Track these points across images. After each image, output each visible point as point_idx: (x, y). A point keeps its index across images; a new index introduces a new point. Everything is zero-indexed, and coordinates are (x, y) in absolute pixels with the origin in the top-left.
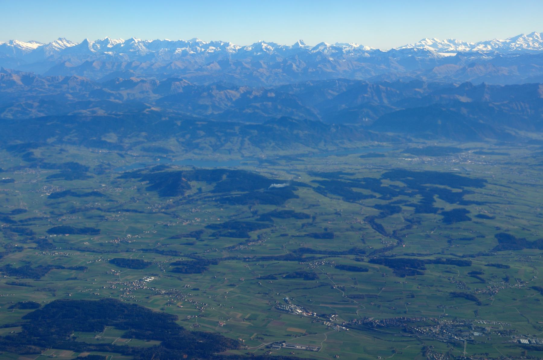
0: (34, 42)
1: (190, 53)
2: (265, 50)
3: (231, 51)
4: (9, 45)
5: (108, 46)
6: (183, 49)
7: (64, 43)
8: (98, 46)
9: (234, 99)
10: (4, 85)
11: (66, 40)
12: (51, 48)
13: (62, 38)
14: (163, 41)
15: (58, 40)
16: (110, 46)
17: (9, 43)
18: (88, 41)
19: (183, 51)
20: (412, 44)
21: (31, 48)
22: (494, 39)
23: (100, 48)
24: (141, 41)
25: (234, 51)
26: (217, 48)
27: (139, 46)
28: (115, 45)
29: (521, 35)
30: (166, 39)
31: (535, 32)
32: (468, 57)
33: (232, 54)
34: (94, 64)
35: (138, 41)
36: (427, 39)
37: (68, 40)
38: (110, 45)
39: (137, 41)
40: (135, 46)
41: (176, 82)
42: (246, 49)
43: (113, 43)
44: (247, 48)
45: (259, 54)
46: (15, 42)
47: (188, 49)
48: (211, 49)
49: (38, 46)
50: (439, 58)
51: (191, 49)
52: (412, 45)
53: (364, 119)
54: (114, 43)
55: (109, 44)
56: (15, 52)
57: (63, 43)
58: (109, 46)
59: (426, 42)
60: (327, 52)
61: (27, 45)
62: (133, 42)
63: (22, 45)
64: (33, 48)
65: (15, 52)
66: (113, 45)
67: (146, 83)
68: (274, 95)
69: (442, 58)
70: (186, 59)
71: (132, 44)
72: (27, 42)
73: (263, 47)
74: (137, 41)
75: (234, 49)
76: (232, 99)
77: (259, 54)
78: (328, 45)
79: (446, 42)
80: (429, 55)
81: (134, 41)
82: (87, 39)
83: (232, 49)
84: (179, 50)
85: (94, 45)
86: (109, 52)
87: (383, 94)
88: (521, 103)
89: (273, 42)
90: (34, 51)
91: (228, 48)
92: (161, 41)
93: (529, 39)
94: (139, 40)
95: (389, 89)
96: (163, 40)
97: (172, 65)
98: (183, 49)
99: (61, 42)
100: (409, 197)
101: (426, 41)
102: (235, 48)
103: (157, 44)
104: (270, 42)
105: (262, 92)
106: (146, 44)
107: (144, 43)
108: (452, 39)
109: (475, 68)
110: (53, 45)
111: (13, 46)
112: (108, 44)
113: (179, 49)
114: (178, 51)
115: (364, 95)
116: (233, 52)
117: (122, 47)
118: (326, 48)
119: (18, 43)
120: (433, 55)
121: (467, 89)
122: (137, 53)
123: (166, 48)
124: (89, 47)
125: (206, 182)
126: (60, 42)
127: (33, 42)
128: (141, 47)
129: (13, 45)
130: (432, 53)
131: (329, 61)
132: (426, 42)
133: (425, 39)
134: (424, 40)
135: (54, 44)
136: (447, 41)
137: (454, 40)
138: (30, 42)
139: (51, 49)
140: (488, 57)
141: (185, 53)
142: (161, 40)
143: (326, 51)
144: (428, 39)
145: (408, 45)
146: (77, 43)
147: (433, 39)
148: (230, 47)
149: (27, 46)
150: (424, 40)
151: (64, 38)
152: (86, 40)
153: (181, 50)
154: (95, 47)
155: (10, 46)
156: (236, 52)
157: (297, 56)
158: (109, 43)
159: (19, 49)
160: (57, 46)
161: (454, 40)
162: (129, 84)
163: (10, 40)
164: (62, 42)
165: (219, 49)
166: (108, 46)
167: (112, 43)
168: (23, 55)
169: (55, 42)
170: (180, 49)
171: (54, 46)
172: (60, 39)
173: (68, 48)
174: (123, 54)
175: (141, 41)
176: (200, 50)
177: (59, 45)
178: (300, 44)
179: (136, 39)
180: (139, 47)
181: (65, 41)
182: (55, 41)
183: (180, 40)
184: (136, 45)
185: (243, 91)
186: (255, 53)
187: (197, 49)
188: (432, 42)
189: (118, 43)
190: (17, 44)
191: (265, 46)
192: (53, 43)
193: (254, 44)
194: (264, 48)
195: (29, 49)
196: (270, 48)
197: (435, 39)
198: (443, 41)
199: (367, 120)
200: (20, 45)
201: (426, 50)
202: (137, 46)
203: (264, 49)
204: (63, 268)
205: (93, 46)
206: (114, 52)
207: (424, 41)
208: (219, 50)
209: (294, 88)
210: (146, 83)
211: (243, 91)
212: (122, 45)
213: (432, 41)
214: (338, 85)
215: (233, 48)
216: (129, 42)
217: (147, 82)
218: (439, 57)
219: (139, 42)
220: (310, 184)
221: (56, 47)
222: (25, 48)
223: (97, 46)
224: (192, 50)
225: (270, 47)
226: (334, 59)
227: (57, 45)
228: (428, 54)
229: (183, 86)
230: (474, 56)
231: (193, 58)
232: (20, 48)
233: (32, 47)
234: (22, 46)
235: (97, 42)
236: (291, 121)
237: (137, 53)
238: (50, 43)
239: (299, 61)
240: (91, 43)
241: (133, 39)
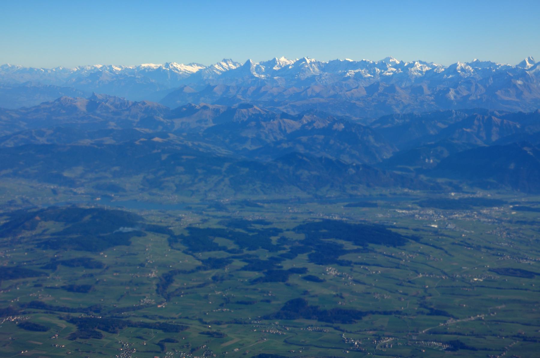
0: (196, 65)
1: (366, 76)
2: (459, 72)
3: (416, 74)
4: (164, 68)
5: (274, 68)
6: (357, 71)
7: (229, 65)
8: (262, 68)
9: (289, 131)
10: (64, 112)
11: (232, 62)
12: (211, 71)
13: (228, 60)
14: (343, 61)
15: (223, 61)
16: (277, 68)
17: (165, 67)
18: (251, 62)
19: (356, 73)
21: (189, 72)
23: (264, 70)
24: (315, 61)
25: (420, 74)
26: (397, 70)
27: (310, 68)
28: (283, 67)
30: (346, 59)
33: (416, 77)
34: (215, 89)
35: (311, 61)
37: (234, 61)
38: (277, 66)
39: (310, 62)
40: (305, 68)
41: (242, 110)
42: (436, 70)
43: (281, 65)
44: (438, 69)
45: (451, 76)
46: (172, 65)
47: (364, 71)
48: (389, 71)
49: (199, 69)
51: (367, 71)
53: (427, 160)
54: (282, 64)
55: (276, 66)
56: (169, 77)
57: (229, 65)
58: (276, 68)
61: (186, 69)
62: (304, 62)
63: (180, 69)
64: (192, 72)
65: (169, 77)
66: (281, 66)
67: (208, 110)
68: (343, 127)
70: (345, 84)
71: (302, 64)
72: (187, 65)
73: (458, 68)
74: (310, 62)
75: (420, 71)
76: (285, 131)
77: (451, 76)
81: (306, 61)
82: (250, 60)
83: (418, 71)
84: (351, 73)
85: (258, 66)
86: (261, 75)
87: (494, 128)
89: (490, 61)
90: (193, 75)
91: (413, 69)
92: (340, 61)
94: (313, 60)
95: (505, 121)
96: (343, 60)
97: (308, 90)
98: (357, 71)
99: (225, 64)
100: (268, 251)
102: (422, 70)
103: (334, 65)
104: (487, 61)
105: (329, 122)
106: (322, 66)
107: (319, 64)
110: (215, 68)
111: (168, 69)
112: (275, 65)
113: (351, 72)
114: (350, 73)
115: (465, 129)
116: (418, 75)
117: (290, 69)
119: (175, 66)
122: (296, 76)
123: (345, 70)
124: (251, 69)
126: (224, 64)
127: (194, 65)
128: (314, 69)
129: (169, 68)
131: (515, 86)
135: (216, 66)
138: (191, 65)
139: (210, 72)
141: (358, 76)
142: (341, 60)
146: (120, 67)
148: (416, 68)
149: (186, 70)
151: (231, 60)
152: (248, 62)
153: (354, 72)
154: (258, 69)
155: (165, 69)
156: (422, 74)
157: (492, 79)
158: (277, 64)
159: (176, 73)
160: (219, 69)
162: (191, 110)
163: (167, 63)
164: (227, 64)
165: (400, 71)
166: (274, 68)
167: (280, 64)
168: (179, 80)
169: (218, 65)
170: (353, 71)
171: (216, 69)
172: (225, 61)
173: (231, 70)
174: (279, 77)
175: (315, 61)
176: (380, 72)
177: (223, 68)
178: (527, 62)
179: (308, 59)
180: (311, 69)
181: (231, 62)
182: (218, 63)
183: (364, 60)
184: (307, 66)
185: (307, 121)
186: (445, 76)
187: (375, 70)
189: (159, 66)
190: (174, 67)
191: (461, 67)
192: (215, 65)
194: (460, 69)
195: (188, 73)
196: (469, 68)
199: (431, 161)
200: (178, 69)
202: (308, 68)
203: (459, 70)
204: (492, 350)
205: (255, 68)
206: (267, 76)
208: (401, 73)
209: (396, 120)
210: (208, 110)
211: (307, 121)
212: (290, 67)
214: (454, 116)
215: (419, 69)
216: (299, 65)
217: (209, 109)
219: (311, 63)
221: (218, 70)
222: (183, 72)
223: (261, 68)
224: (369, 73)
225: (469, 67)
226: (524, 83)
227: (220, 68)
229: (250, 114)
231: (357, 82)
232: (176, 71)
233: (192, 71)
234: (179, 70)
235: (262, 63)
236: (300, 157)
237: (296, 76)
238: (212, 65)
239: (476, 85)
240: (255, 63)
241: (305, 59)
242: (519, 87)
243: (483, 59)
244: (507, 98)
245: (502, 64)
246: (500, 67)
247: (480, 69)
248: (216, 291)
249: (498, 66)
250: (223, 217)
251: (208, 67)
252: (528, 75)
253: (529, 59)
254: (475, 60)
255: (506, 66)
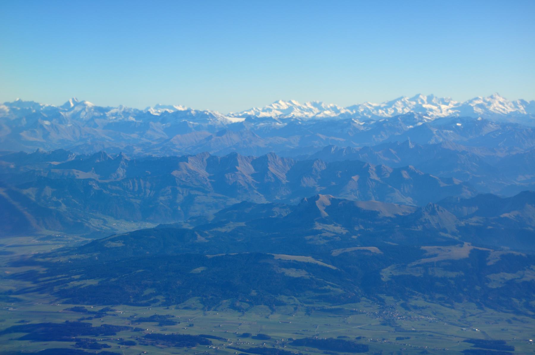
20: (258, 108)
22: (365, 103)
29: (400, 99)
31: (419, 95)
32: (256, 123)
36: (281, 102)
50: (223, 124)
52: (258, 109)
59: (278, 105)
60: (85, 115)
69: (228, 125)
78: (89, 104)
79: (310, 106)
80: (210, 120)
88: (141, 181)
93: (410, 104)
101: (279, 104)
108: (318, 102)
109: (224, 137)
118: (84, 109)
120: (216, 120)
121: (98, 161)
125: (93, 326)
130: (214, 117)
131: (42, 126)
132: (278, 105)
133: (279, 101)
134: (277, 102)
136: (310, 104)
137: (321, 103)
140: (283, 124)
143: (83, 114)
144: (283, 101)
145: (252, 109)
147: (290, 102)
150: (277, 102)
161: (321, 103)
188: (288, 105)
193: (19, 103)
197: (294, 102)
198: (305, 104)
201: (208, 114)
207: (276, 104)
213: (288, 104)
218: (223, 123)
220: (9, 308)
225: (351, 113)
228: (209, 118)
230: (263, 123)
242: (46, 127)
243: (26, 98)
244: (31, 139)
245: (47, 105)
246: (44, 107)
247: (19, 109)
248: (313, 167)
249: (42, 107)
250: (501, 112)
251: (72, 105)
252: (63, 116)
253: (73, 99)
254: (18, 99)
255: (50, 107)
